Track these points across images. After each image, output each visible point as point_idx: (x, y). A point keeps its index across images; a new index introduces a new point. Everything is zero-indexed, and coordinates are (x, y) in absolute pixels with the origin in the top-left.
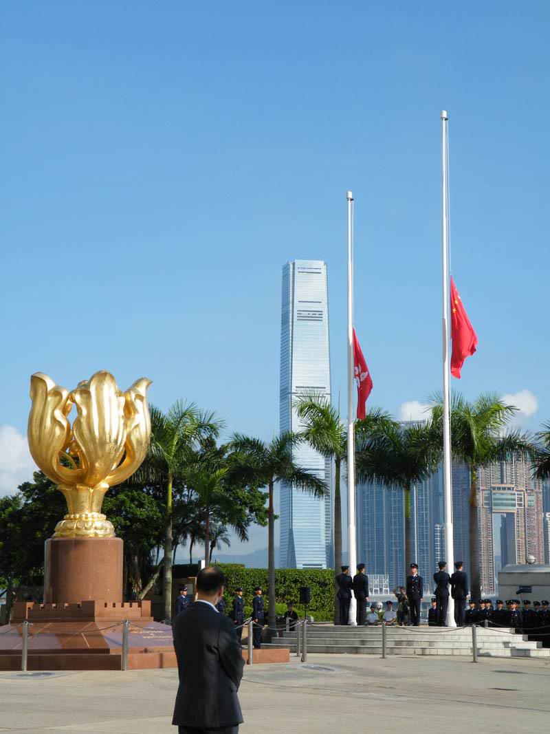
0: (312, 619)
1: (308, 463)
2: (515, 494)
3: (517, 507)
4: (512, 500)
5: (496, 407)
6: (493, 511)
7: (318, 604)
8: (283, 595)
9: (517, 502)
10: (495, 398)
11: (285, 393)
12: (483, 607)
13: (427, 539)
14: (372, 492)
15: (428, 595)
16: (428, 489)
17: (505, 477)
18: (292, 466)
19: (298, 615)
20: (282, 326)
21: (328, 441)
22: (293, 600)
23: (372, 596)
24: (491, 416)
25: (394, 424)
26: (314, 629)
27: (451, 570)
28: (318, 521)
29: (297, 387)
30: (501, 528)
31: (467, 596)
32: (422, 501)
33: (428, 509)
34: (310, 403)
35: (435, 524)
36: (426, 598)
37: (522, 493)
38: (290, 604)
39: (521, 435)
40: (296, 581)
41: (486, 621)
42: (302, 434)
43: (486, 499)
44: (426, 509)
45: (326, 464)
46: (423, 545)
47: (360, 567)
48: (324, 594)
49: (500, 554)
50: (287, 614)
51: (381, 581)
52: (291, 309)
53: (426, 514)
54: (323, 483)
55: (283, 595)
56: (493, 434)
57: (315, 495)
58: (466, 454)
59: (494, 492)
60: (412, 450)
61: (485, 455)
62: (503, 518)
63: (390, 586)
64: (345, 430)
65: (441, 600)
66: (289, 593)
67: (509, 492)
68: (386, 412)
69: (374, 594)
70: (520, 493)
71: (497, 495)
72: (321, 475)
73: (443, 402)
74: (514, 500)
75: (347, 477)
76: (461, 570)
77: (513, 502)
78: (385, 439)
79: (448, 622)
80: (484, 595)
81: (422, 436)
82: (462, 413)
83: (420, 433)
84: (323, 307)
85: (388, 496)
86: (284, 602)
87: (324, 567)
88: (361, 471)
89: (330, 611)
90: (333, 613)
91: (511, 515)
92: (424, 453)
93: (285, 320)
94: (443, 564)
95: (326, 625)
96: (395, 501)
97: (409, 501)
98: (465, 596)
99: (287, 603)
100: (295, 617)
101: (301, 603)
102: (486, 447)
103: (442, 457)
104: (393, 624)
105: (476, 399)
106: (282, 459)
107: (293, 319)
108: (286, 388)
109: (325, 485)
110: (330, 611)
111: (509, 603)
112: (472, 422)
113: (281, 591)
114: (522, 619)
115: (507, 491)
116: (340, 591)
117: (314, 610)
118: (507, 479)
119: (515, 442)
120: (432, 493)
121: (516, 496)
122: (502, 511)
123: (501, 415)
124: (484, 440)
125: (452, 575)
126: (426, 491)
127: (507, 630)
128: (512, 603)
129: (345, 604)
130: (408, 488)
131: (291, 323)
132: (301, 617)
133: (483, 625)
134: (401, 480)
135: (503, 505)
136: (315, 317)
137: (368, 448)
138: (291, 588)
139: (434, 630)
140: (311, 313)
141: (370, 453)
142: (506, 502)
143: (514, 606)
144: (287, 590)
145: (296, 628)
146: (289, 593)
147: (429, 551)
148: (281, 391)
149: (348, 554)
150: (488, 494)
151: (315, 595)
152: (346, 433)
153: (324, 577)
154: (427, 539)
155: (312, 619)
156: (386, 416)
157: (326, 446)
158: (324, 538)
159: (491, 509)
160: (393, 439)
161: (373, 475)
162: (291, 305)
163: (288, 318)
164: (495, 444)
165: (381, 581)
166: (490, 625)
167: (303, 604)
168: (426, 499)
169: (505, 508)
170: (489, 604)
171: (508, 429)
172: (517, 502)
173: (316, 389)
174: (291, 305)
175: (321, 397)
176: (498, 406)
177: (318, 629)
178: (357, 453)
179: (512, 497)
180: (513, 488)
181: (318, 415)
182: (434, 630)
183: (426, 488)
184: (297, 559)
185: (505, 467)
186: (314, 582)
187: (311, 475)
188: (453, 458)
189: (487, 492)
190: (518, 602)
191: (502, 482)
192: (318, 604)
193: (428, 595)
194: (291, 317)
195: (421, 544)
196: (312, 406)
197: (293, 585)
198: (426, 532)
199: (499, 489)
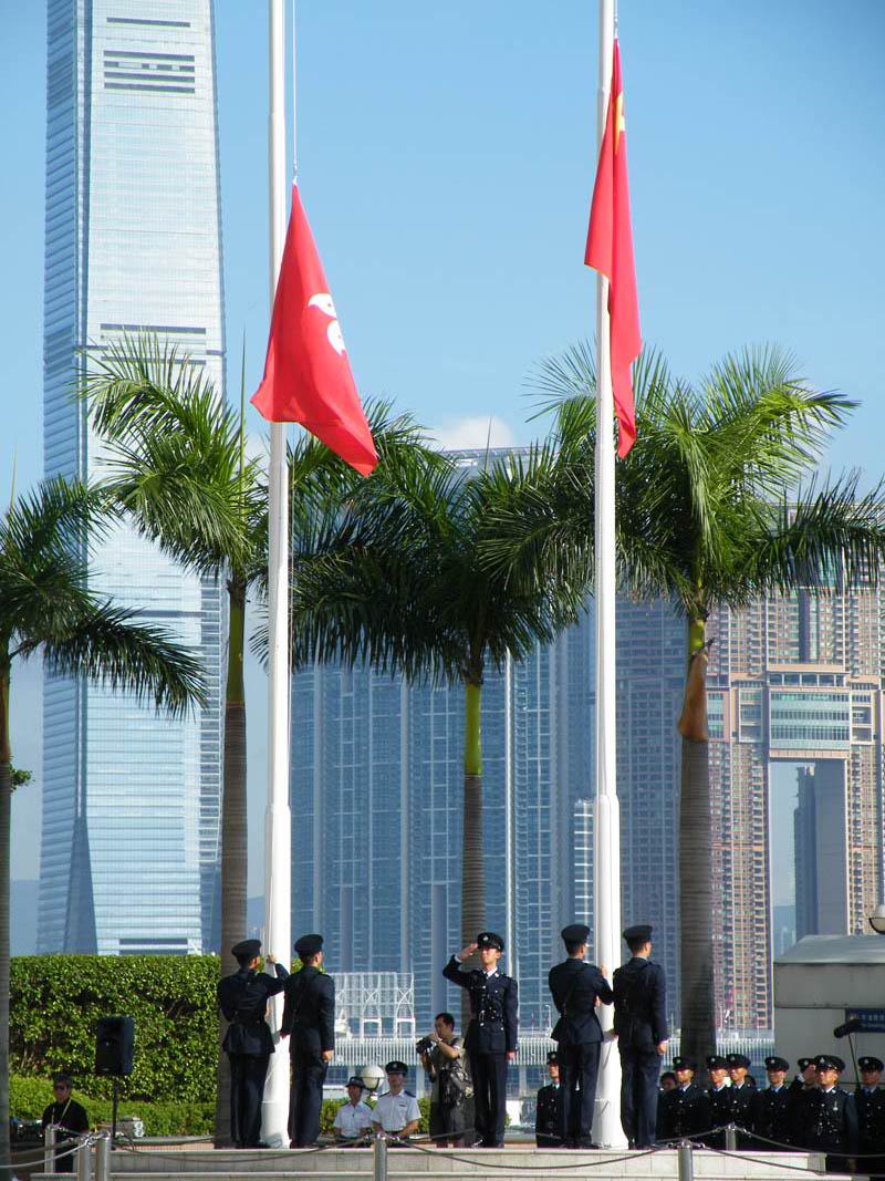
0: (139, 1127)
1: (144, 593)
2: (844, 698)
3: (853, 740)
4: (836, 716)
5: (778, 403)
6: (772, 754)
7: (159, 1076)
8: (39, 1049)
9: (851, 726)
10: (773, 370)
11: (63, 347)
12: (724, 1080)
13: (546, 851)
14: (362, 692)
15: (535, 1041)
16: (552, 678)
17: (813, 641)
18: (81, 599)
19: (91, 1114)
20: (49, 109)
21: (203, 514)
22: (76, 1064)
23: (347, 1042)
24: (760, 433)
25: (434, 458)
26: (143, 1163)
27: (610, 956)
28: (176, 790)
29: (105, 327)
30: (797, 813)
31: (664, 1045)
32: (533, 722)
33: (553, 750)
34: (142, 385)
35: (573, 799)
36: (528, 1051)
37: (872, 693)
38: (63, 1079)
39: (860, 497)
40: (84, 999)
41: (731, 1128)
42: (110, 490)
43: (749, 712)
44: (545, 747)
45: (205, 594)
46: (534, 868)
47: (305, 947)
48: (183, 1039)
49: (792, 901)
50: (53, 1113)
51: (387, 995)
52: (81, 45)
53: (545, 763)
54: (186, 661)
55: (39, 1049)
56: (766, 493)
57: (159, 701)
58: (673, 560)
59: (773, 689)
60: (491, 549)
61: (738, 566)
62: (803, 778)
63: (417, 1009)
64: (262, 480)
65: (576, 1058)
66: (61, 1040)
67: (829, 689)
68: (405, 417)
69: (362, 1041)
70: (865, 693)
71: (786, 700)
72: (187, 635)
73: (595, 382)
74: (844, 716)
75: (265, 641)
76: (644, 954)
77: (840, 723)
78: (399, 510)
79: (599, 1133)
80: (728, 1040)
81: (525, 497)
82: (662, 423)
83: (517, 489)
84: (196, 43)
85: (419, 706)
86: (41, 1071)
87: (195, 948)
88: (318, 617)
89: (203, 1099)
90: (210, 1106)
91: (831, 767)
92: (531, 557)
93: (62, 84)
94: (576, 936)
95: (187, 1149)
96: (440, 721)
97: (475, 728)
98: (657, 1042)
99: (53, 1076)
100: (76, 1121)
101: (98, 1073)
102: (741, 539)
103: (585, 573)
104: (408, 1143)
105: (710, 372)
106: (40, 578)
107: (88, 83)
108: (68, 329)
109: (190, 666)
110: (203, 1099)
111: (820, 1064)
112: (694, 453)
113: (33, 1033)
114: (853, 1119)
115: (817, 688)
116: (232, 1031)
117: (147, 1099)
118: (820, 645)
119: (837, 521)
120: (565, 694)
121: (851, 704)
122: (801, 755)
123: (796, 428)
124: (733, 511)
125: (617, 973)
126: (545, 686)
127: (799, 1159)
128: (824, 1068)
129: (249, 1073)
130: (473, 676)
131: (81, 99)
132: (97, 1121)
133: (718, 1144)
134: (451, 652)
135: (802, 733)
136: (169, 76)
137: (341, 542)
138: (68, 1020)
139: (554, 1161)
140: (154, 62)
141: (349, 556)
142: (816, 723)
143: (830, 1077)
144: (53, 1029)
145: (77, 1163)
146: (61, 1040)
147: (555, 890)
148: (48, 338)
149: (264, 903)
150: (756, 696)
151: (150, 1046)
152: (265, 489)
153: (184, 983)
154: (546, 851)
155: (139, 1127)
156: (405, 433)
157: (196, 533)
158: (197, 849)
159: (765, 747)
160: (428, 502)
161: (357, 629)
162: (81, 32)
163: (72, 74)
164: (772, 526)
165: (387, 995)
166: (744, 1144)
167: (107, 1074)
168: (544, 715)
169: (810, 743)
170: (742, 1071)
171: (815, 475)
172: (851, 726)
173: (162, 335)
174: (81, 32)
175: (182, 362)
176: (786, 396)
177: (156, 1162)
178: (299, 559)
179: (838, 706)
180: (840, 678)
181: (167, 430)
182: (554, 1161)
183: (545, 675)
184: (98, 921)
185: (813, 607)
186: (151, 1000)
187: (143, 633)
188: (625, 575)
189: (753, 690)
190: (839, 1065)
191: (803, 657)
192: (159, 1076)
193: (535, 1041)
194: (81, 76)
195: (526, 868)
196: (148, 396)
197: (76, 1013)
198: (545, 826)
199: (792, 678)
